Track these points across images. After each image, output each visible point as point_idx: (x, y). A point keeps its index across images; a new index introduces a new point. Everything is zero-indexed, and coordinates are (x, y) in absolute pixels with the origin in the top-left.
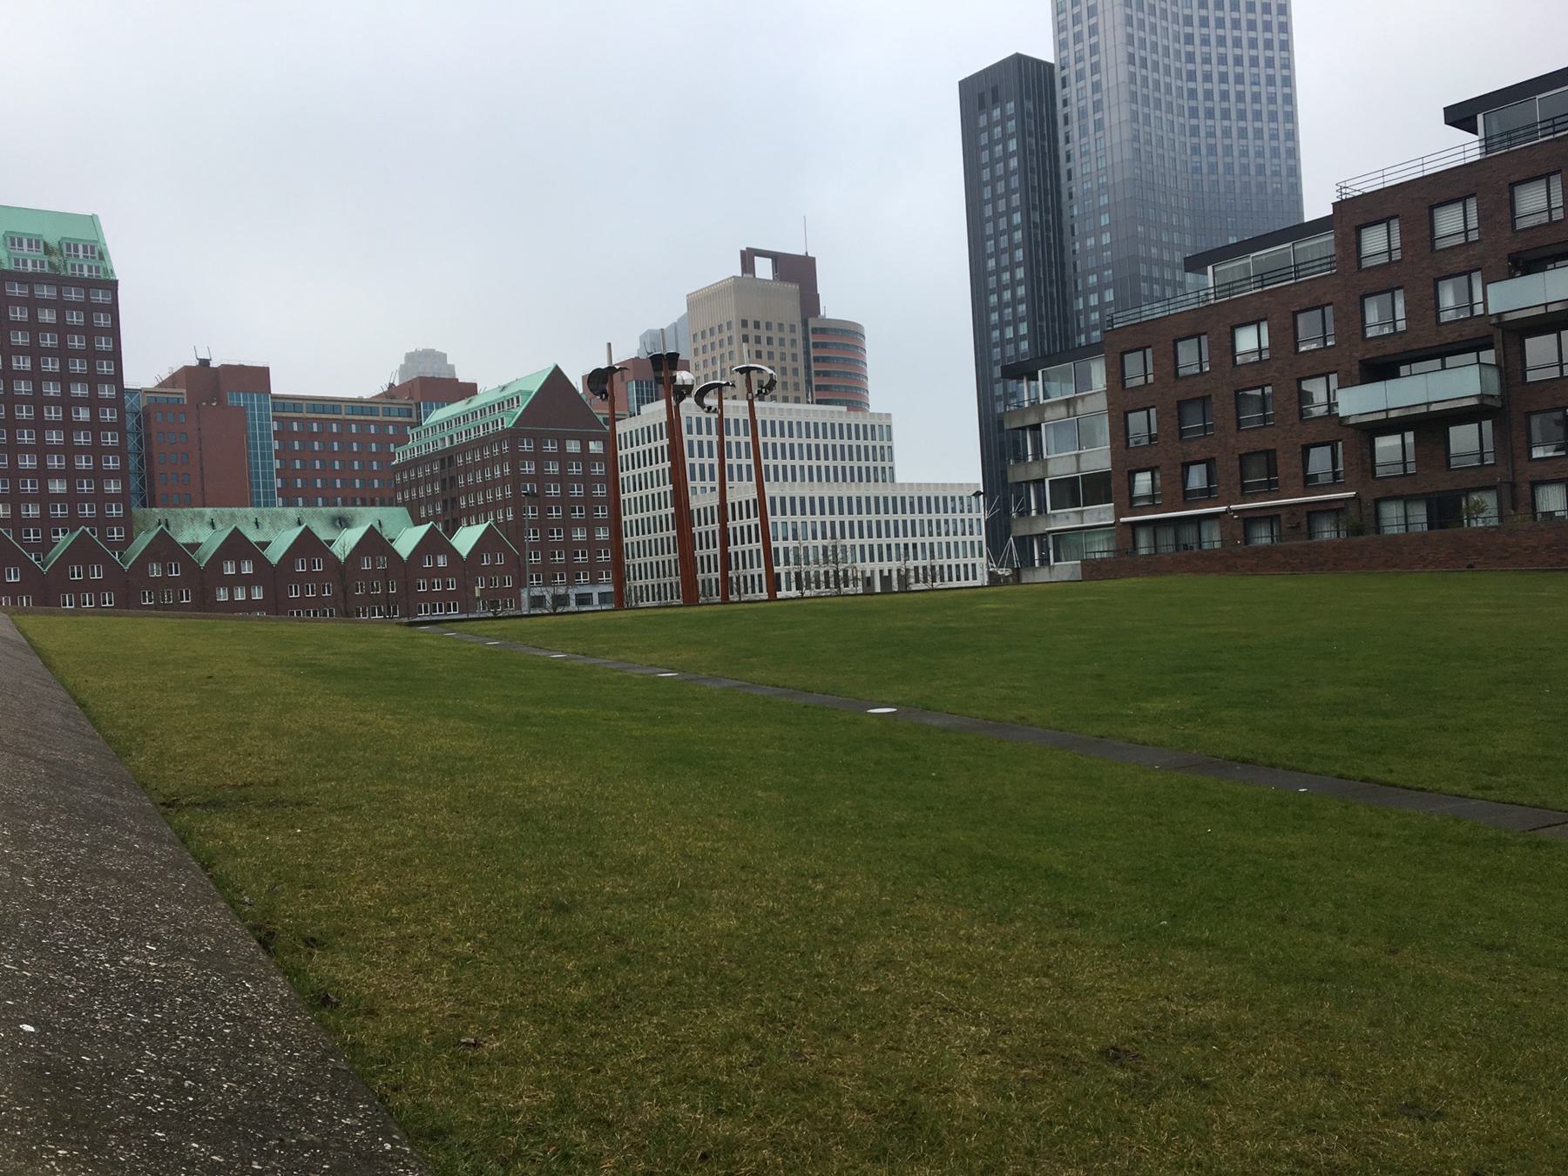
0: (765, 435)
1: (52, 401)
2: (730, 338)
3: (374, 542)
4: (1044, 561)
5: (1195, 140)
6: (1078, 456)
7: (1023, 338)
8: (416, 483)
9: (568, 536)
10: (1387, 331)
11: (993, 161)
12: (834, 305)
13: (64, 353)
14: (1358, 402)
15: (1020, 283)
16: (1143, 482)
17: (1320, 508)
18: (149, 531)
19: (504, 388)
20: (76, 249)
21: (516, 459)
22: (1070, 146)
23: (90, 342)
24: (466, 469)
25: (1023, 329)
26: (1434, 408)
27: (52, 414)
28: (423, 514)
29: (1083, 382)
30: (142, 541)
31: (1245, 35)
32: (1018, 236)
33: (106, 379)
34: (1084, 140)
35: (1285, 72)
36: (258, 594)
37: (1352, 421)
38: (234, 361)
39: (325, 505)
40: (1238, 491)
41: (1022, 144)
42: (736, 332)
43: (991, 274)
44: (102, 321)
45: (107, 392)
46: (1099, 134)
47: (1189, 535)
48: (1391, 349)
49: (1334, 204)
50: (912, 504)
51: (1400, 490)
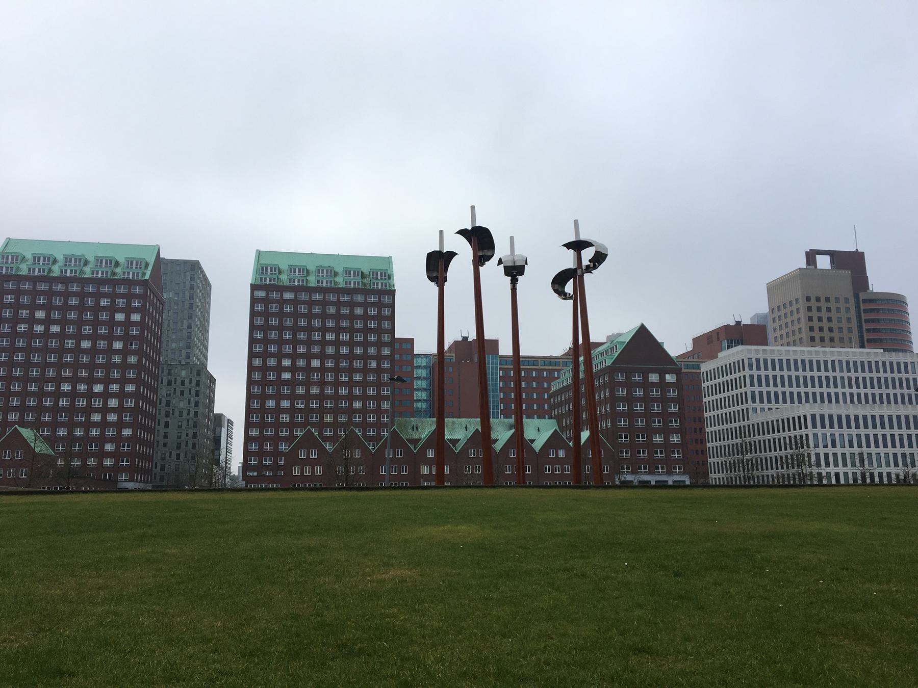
12: (879, 281)
13: (365, 331)
36: (319, 471)
42: (802, 305)
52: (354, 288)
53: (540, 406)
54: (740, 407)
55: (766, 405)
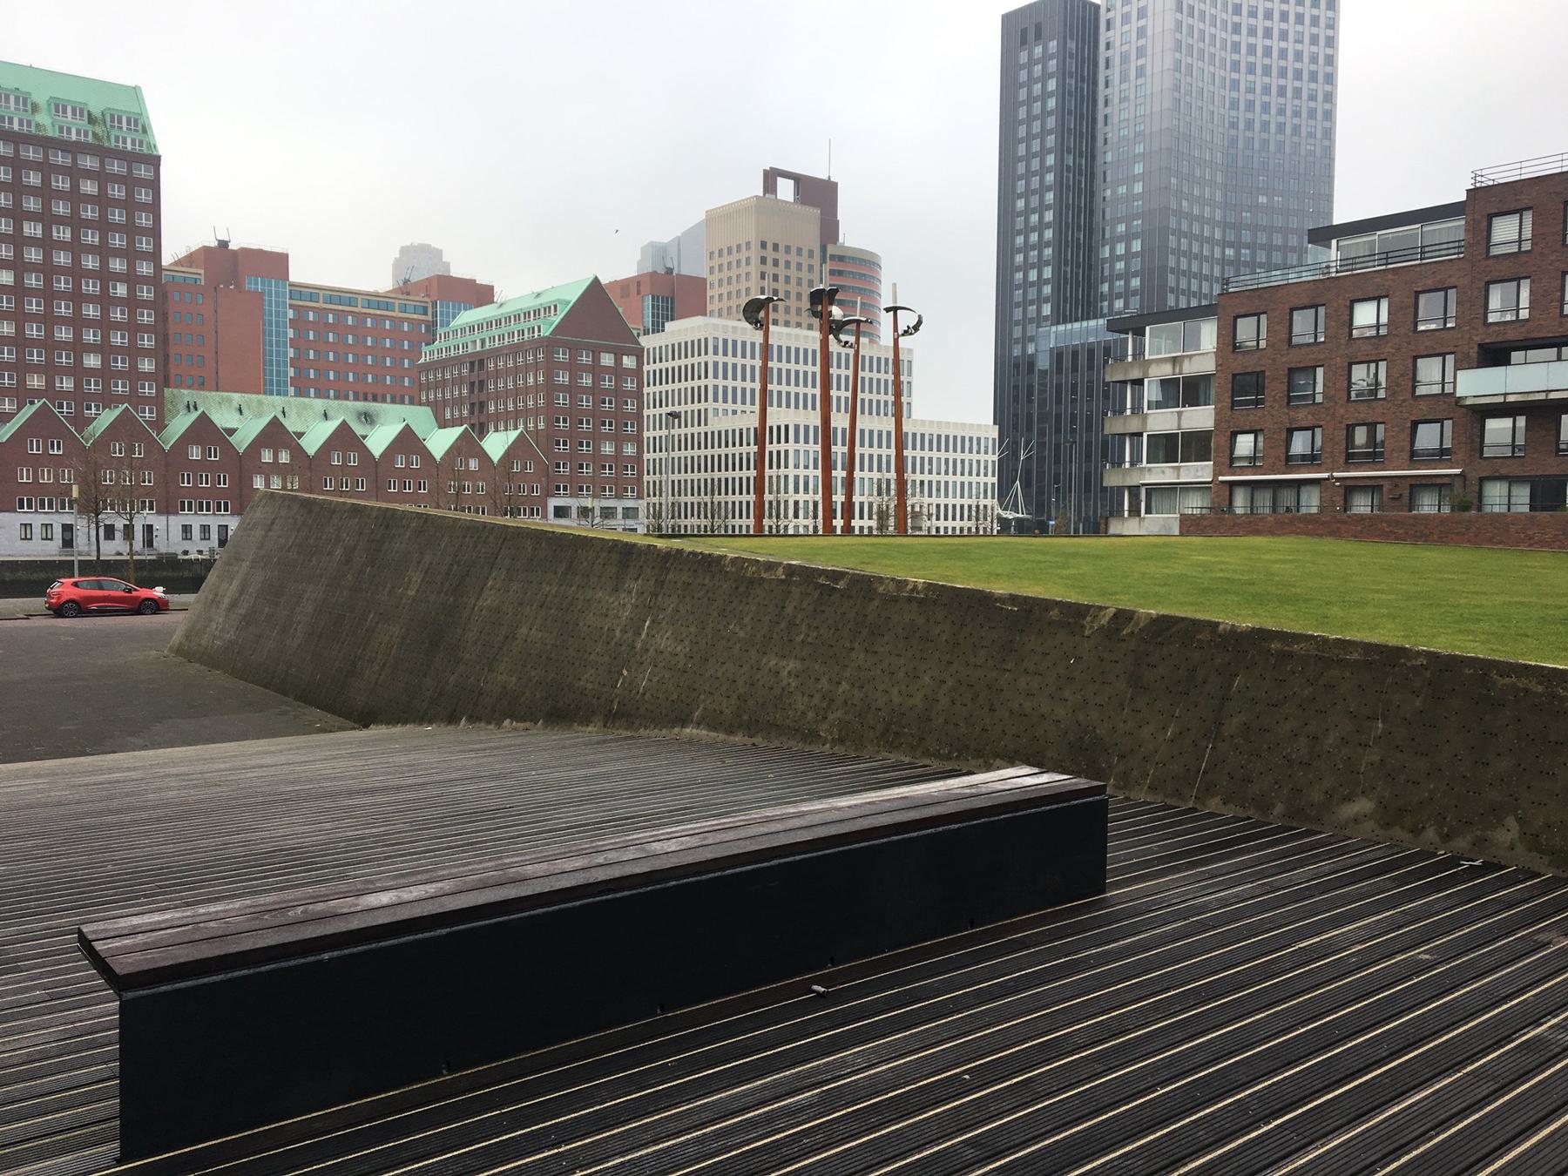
1: (90, 274)
2: (748, 259)
3: (408, 441)
4: (1135, 512)
7: (1047, 282)
8: (443, 384)
9: (597, 449)
10: (1508, 317)
11: (1031, 99)
12: (851, 236)
13: (104, 226)
14: (1476, 384)
15: (1048, 226)
16: (1245, 444)
19: (538, 295)
20: (120, 122)
21: (550, 369)
22: (1109, 91)
23: (130, 217)
24: (497, 374)
25: (1048, 273)
26: (1552, 396)
27: (90, 287)
28: (448, 416)
29: (1192, 340)
30: (180, 424)
32: (1050, 178)
33: (145, 256)
34: (1124, 86)
37: (1468, 402)
38: (254, 244)
39: (337, 397)
40: (1342, 460)
41: (1062, 85)
42: (755, 253)
43: (1019, 214)
44: (143, 196)
46: (1140, 81)
47: (1287, 498)
48: (1511, 335)
49: (1468, 191)
50: (931, 441)
53: (398, 380)
54: (696, 406)
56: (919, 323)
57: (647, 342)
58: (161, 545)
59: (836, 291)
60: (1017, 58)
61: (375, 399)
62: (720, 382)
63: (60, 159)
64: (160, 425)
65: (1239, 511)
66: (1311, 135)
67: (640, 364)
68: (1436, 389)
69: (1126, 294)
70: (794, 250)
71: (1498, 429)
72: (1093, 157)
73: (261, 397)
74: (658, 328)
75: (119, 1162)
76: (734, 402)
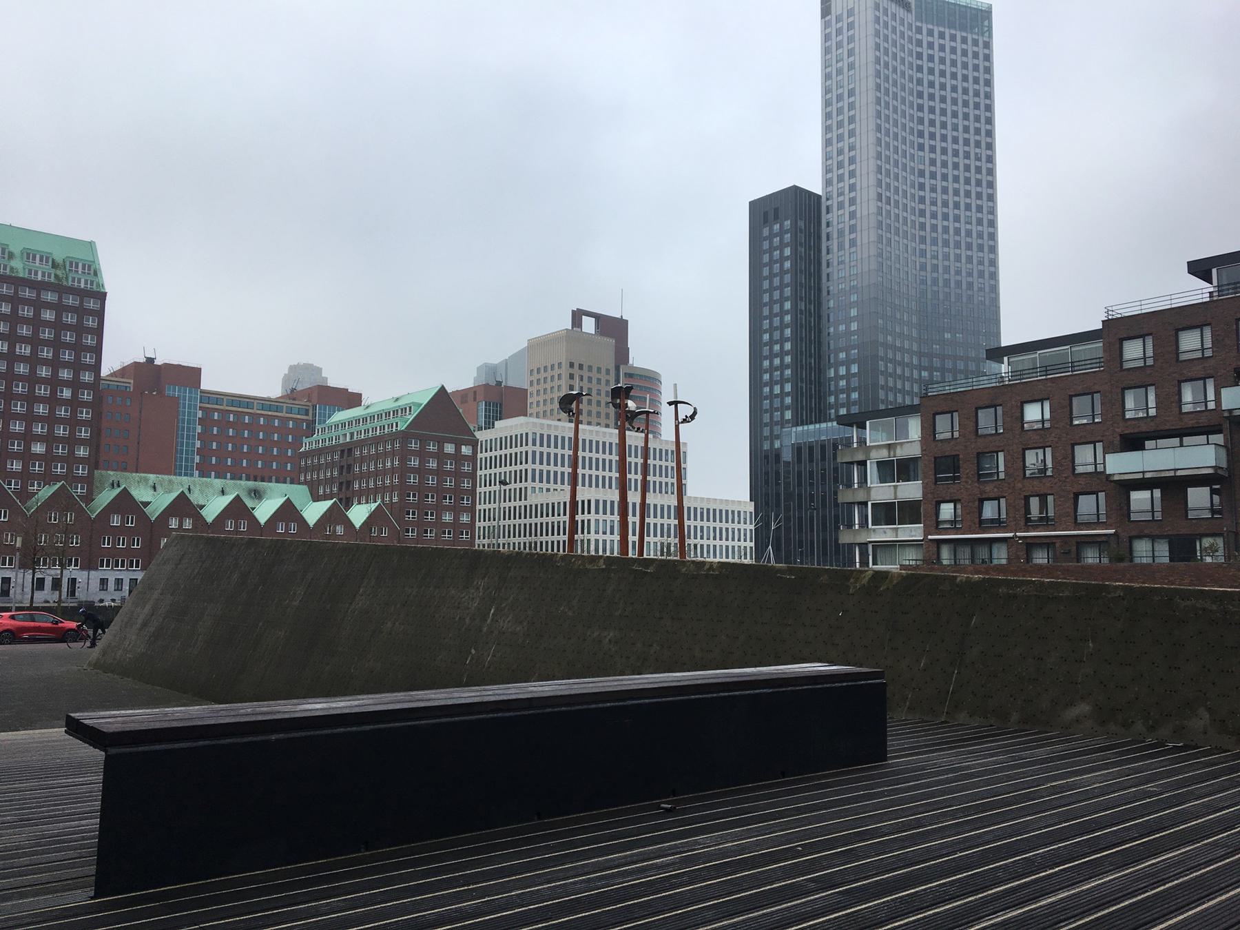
0: (584, 450)
3: (288, 511)
5: (923, 260)
6: (895, 487)
8: (318, 468)
9: (439, 517)
10: (1141, 415)
11: (772, 262)
12: (639, 357)
13: (57, 344)
14: (1120, 464)
16: (947, 511)
17: (1038, 541)
18: (170, 491)
19: (397, 399)
20: (77, 267)
21: (404, 456)
22: (830, 256)
24: (362, 459)
26: (1179, 473)
28: (321, 492)
29: (903, 431)
30: (106, 497)
31: (951, 186)
32: (788, 318)
34: (841, 253)
35: (990, 217)
37: (1116, 478)
39: (232, 479)
40: (1022, 523)
42: (565, 371)
45: (87, 377)
46: (853, 249)
47: (983, 553)
48: (1144, 428)
50: (702, 514)
51: (1148, 530)
52: (42, 282)
55: (545, 485)
56: (695, 413)
57: (482, 436)
58: (81, 595)
59: (631, 388)
60: (761, 232)
61: (263, 480)
62: (537, 467)
63: (27, 293)
64: (89, 498)
65: (945, 562)
66: (980, 289)
67: (475, 452)
68: (1091, 469)
69: (848, 404)
70: (595, 369)
71: (1139, 498)
72: (820, 304)
73: (173, 477)
74: (489, 425)
75: (92, 898)
76: (548, 482)
